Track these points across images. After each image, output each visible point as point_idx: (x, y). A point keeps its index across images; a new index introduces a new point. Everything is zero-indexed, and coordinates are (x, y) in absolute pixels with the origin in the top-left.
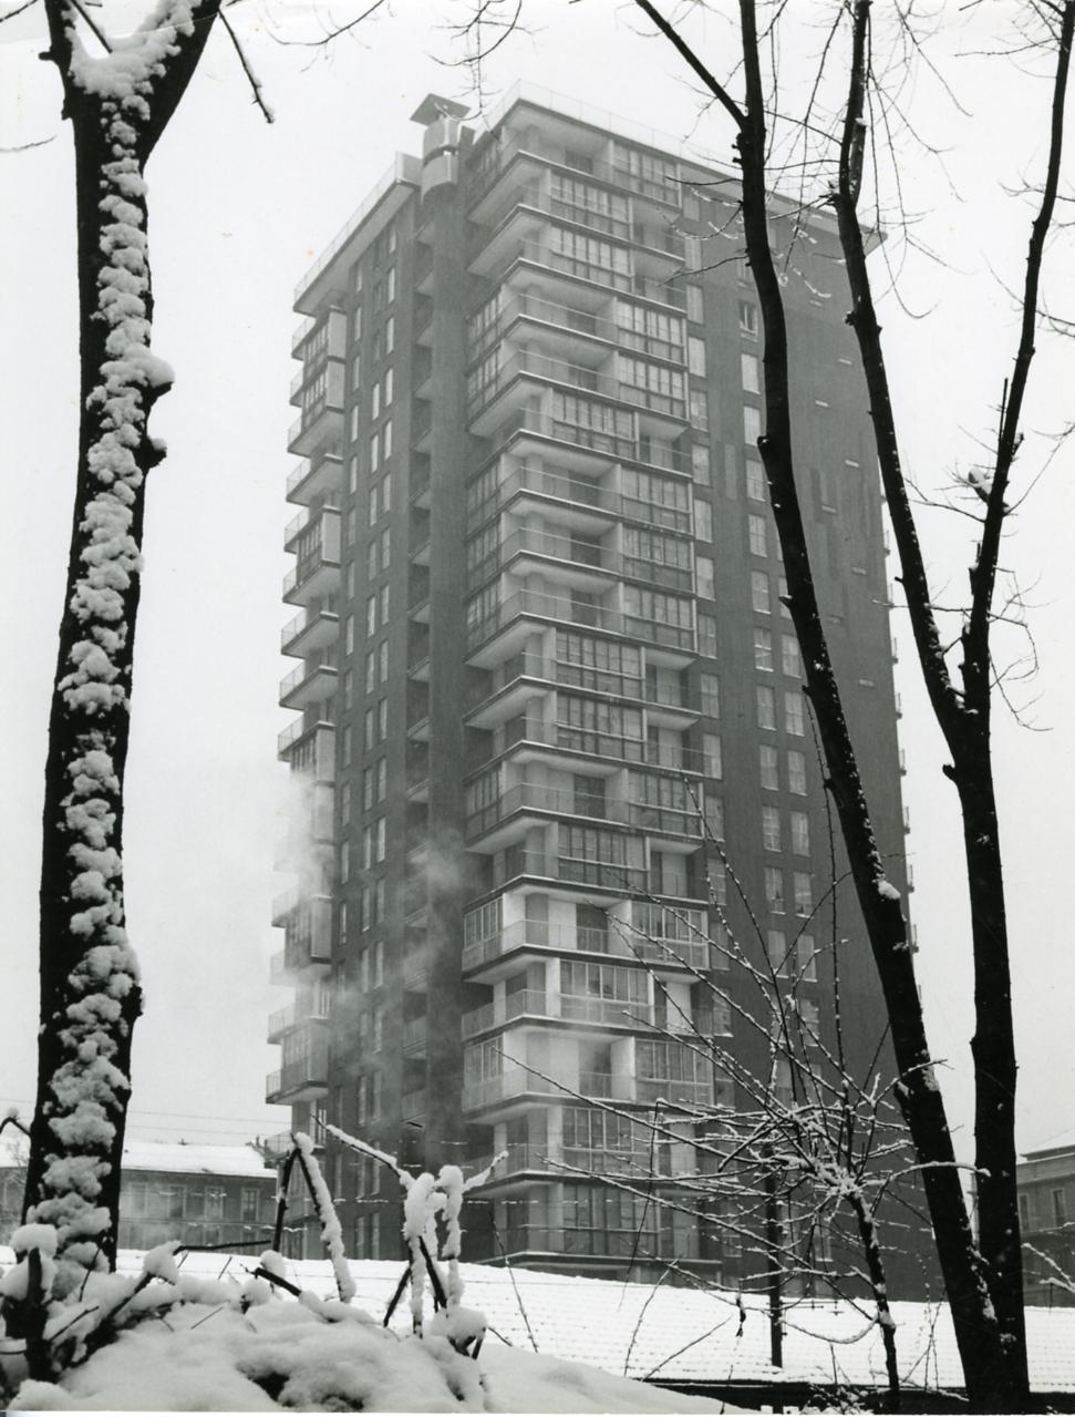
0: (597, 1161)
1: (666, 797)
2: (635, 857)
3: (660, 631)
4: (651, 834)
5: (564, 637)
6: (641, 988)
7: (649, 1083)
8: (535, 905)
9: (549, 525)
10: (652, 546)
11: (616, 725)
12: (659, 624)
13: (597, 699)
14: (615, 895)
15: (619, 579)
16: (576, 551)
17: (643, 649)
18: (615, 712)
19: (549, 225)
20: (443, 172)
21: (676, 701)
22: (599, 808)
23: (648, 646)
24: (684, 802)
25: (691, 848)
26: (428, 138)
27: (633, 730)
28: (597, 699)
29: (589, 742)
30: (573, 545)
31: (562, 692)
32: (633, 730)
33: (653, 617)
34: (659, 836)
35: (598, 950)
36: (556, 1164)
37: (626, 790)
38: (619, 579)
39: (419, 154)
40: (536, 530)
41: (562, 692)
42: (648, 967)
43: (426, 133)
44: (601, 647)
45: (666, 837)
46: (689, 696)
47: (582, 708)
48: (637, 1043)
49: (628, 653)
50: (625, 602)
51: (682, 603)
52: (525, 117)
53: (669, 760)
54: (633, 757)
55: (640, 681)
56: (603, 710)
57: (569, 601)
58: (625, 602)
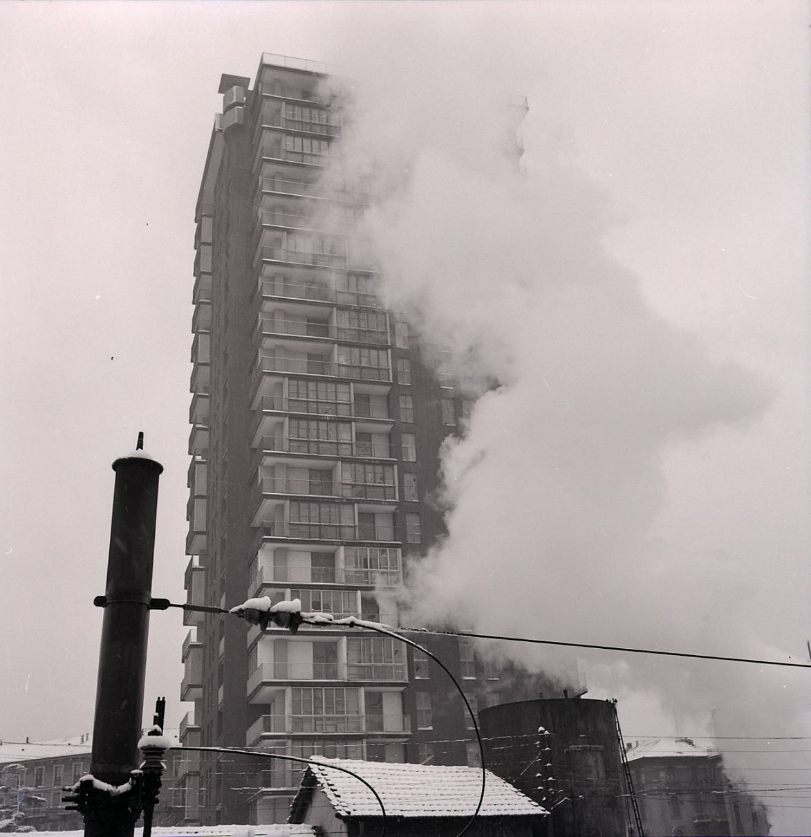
0: (318, 723)
1: (370, 476)
2: (349, 517)
3: (364, 371)
4: (358, 502)
5: (295, 382)
6: (351, 603)
7: (359, 666)
8: (280, 556)
9: (287, 315)
10: (359, 319)
11: (333, 434)
12: (364, 367)
13: (319, 419)
14: (332, 543)
15: (334, 342)
16: (310, 329)
17: (352, 384)
18: (333, 426)
19: (284, 135)
20: (235, 117)
21: (385, 415)
22: (329, 487)
23: (355, 382)
24: (383, 479)
25: (393, 508)
26: (225, 100)
27: (347, 435)
28: (319, 419)
29: (313, 447)
30: (308, 325)
31: (292, 417)
32: (347, 435)
33: (361, 363)
34: (364, 502)
35: (319, 582)
36: (289, 729)
37: (344, 475)
38: (334, 342)
39: (222, 113)
40: (279, 320)
41: (292, 417)
42: (355, 589)
43: (224, 97)
44: (322, 386)
45: (369, 502)
46: (392, 410)
47: (318, 426)
48: (348, 640)
49: (342, 388)
50: (340, 357)
51: (381, 352)
52: (269, 75)
53: (380, 451)
54: (345, 452)
55: (350, 405)
56: (323, 426)
57: (307, 360)
58: (340, 357)
